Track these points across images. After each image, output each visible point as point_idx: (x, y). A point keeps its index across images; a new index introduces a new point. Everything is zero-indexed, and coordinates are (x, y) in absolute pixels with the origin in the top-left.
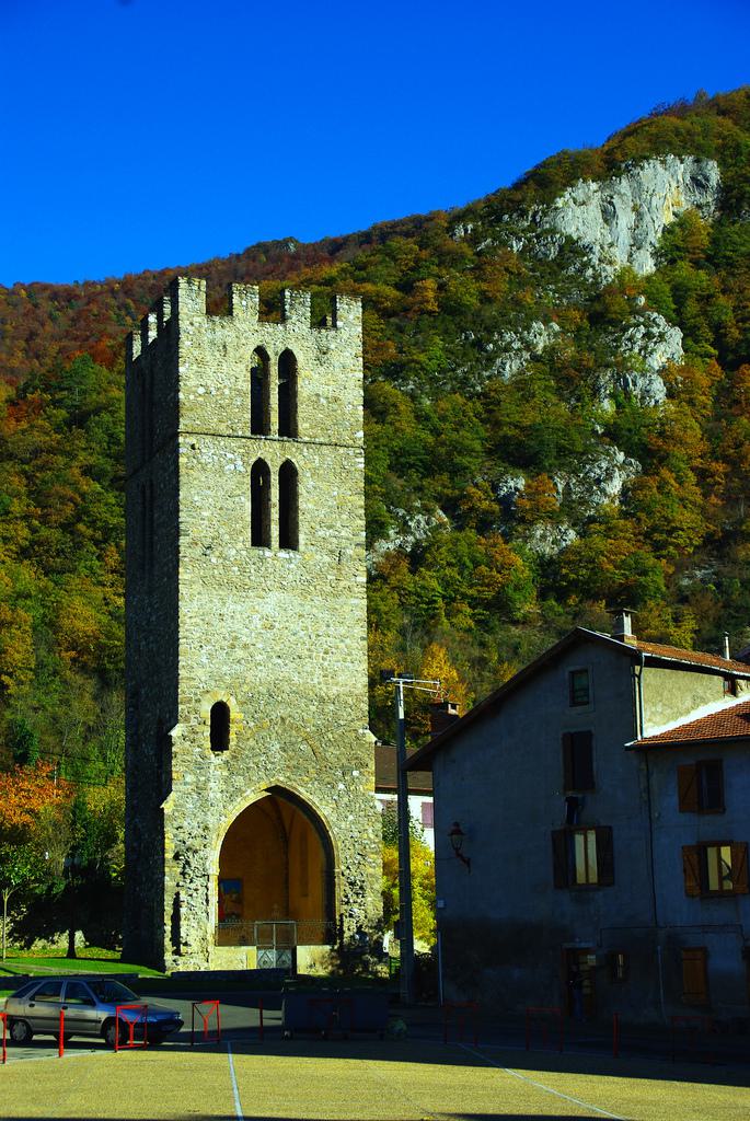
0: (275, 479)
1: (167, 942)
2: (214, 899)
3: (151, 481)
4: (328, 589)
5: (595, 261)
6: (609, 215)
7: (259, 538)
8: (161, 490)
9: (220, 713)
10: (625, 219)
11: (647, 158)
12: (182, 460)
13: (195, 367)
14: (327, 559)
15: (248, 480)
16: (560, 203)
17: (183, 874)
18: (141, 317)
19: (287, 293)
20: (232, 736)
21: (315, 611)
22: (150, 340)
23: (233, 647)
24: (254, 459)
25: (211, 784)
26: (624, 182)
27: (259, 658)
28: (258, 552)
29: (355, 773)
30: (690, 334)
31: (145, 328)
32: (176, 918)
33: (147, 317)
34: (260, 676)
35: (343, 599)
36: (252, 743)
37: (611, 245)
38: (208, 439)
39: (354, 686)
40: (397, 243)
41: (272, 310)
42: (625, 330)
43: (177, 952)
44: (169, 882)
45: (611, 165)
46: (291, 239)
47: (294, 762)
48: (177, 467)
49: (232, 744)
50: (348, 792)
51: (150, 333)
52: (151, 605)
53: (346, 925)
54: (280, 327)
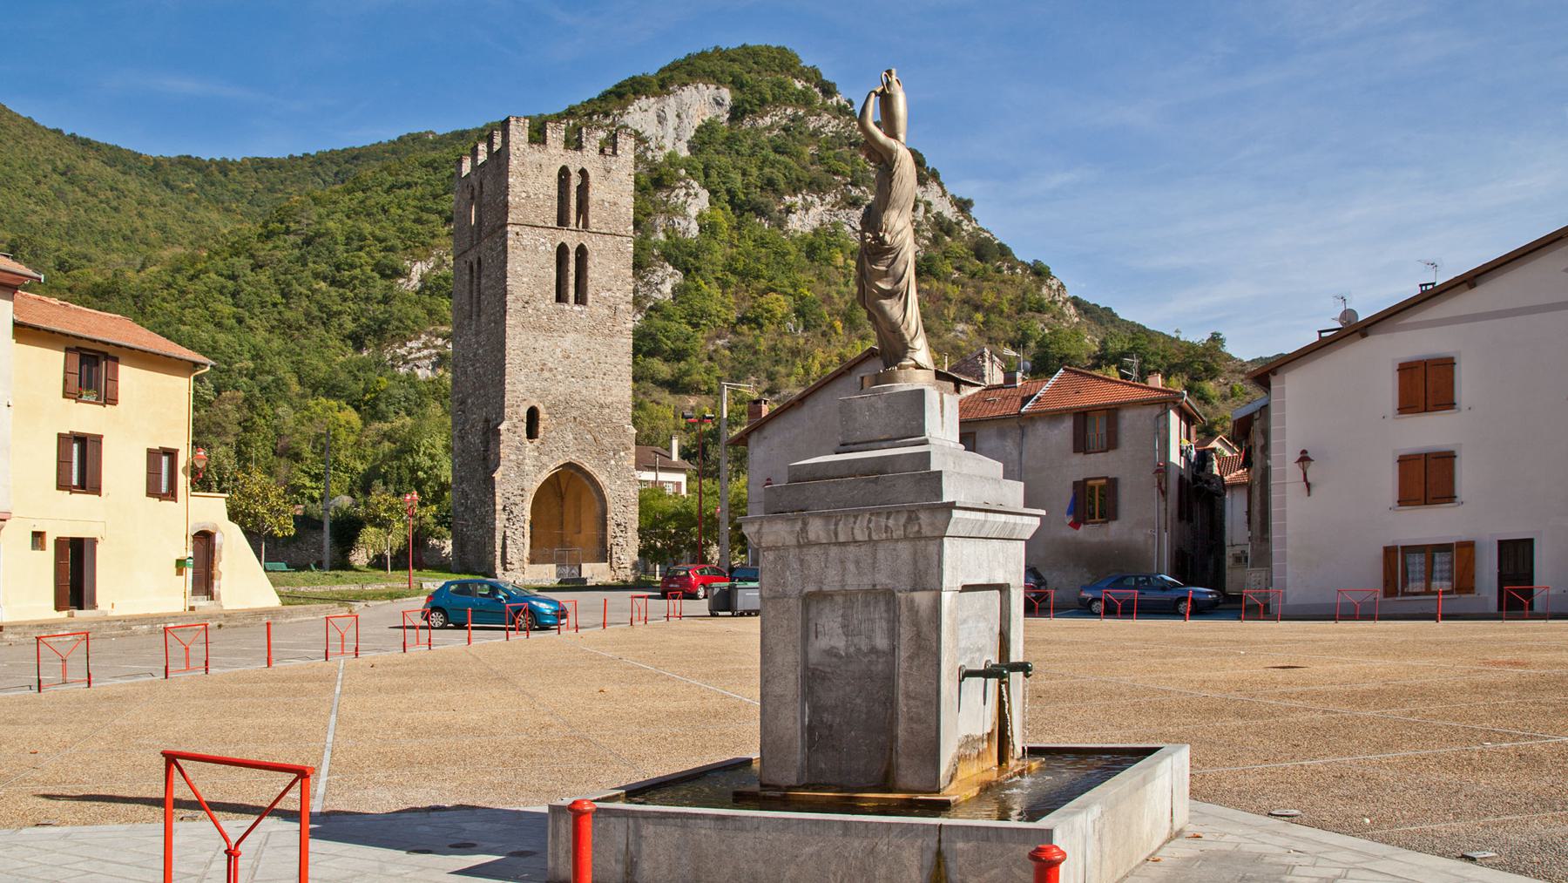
0: (572, 257)
1: (498, 562)
2: (528, 535)
3: (479, 258)
4: (607, 331)
5: (653, 147)
6: (661, 119)
7: (561, 297)
8: (489, 264)
9: (533, 414)
10: (672, 120)
11: (686, 85)
12: (510, 243)
13: (520, 179)
14: (607, 312)
15: (554, 257)
16: (631, 109)
17: (508, 519)
18: (472, 144)
19: (584, 130)
20: (541, 429)
21: (597, 346)
22: (479, 162)
23: (542, 370)
24: (559, 243)
25: (527, 461)
26: (672, 99)
27: (559, 377)
28: (560, 306)
29: (622, 454)
30: (713, 193)
31: (474, 153)
32: (504, 547)
33: (476, 146)
34: (560, 390)
35: (616, 339)
36: (554, 434)
37: (663, 137)
38: (528, 229)
39: (623, 397)
40: (367, 172)
41: (574, 143)
42: (673, 191)
43: (505, 569)
44: (499, 524)
45: (663, 83)
46: (431, 132)
47: (581, 447)
48: (505, 247)
49: (541, 435)
50: (617, 465)
51: (479, 157)
52: (477, 342)
53: (614, 551)
54: (579, 153)
